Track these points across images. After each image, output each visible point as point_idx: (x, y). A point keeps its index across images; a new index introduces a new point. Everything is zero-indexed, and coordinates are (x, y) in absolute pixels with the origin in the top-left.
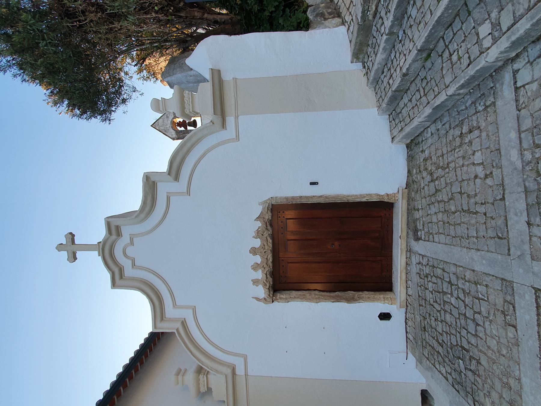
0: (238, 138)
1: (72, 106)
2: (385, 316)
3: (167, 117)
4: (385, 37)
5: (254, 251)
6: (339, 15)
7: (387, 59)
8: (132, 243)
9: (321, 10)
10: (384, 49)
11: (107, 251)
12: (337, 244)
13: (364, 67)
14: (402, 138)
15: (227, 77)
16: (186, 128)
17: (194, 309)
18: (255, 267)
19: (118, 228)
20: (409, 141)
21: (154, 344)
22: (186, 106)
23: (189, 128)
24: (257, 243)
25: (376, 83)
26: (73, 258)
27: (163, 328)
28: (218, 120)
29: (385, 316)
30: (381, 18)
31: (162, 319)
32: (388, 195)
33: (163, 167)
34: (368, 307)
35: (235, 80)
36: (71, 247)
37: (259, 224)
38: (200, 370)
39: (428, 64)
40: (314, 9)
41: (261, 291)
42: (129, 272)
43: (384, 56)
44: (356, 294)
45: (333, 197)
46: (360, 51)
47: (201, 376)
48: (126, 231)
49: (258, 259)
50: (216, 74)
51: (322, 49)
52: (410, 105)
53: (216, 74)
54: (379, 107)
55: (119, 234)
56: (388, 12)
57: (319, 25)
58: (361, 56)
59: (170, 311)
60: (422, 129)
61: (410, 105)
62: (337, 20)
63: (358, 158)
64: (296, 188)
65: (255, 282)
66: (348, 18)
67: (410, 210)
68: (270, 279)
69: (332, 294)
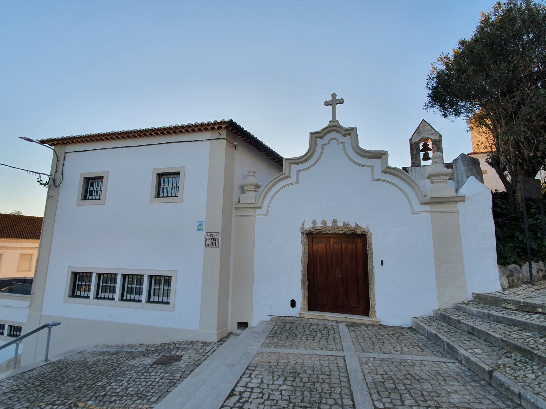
0: (414, 212)
1: (439, 76)
2: (293, 304)
3: (433, 134)
4: (486, 312)
5: (335, 221)
6: (510, 287)
7: (473, 314)
8: (339, 143)
9: (516, 274)
10: (479, 312)
11: (334, 127)
12: (340, 276)
13: (469, 302)
14: (416, 322)
15: (460, 206)
16: (422, 151)
17: (296, 183)
18: (324, 222)
19: (350, 134)
20: (414, 327)
21: (274, 160)
22: (437, 178)
23: (422, 154)
24: (340, 224)
25: (458, 308)
26: (327, 104)
27: (286, 165)
28: (426, 200)
29: (293, 304)
30: (502, 311)
31: (290, 163)
32: (375, 312)
33: (391, 164)
34: (299, 293)
35: (458, 212)
36: (334, 102)
37: (353, 225)
38: (257, 186)
39: (465, 333)
40: (517, 270)
41: (308, 226)
42: (320, 142)
43: (474, 312)
44: (307, 287)
45: (372, 275)
46: (480, 299)
47: (253, 187)
48: (347, 139)
49: (330, 224)
50: (463, 199)
51: (484, 274)
52: (439, 326)
53: (463, 199)
54: (439, 310)
55: (345, 135)
56: (503, 314)
57: (502, 273)
58: (477, 300)
59: (295, 168)
60: (422, 333)
61: (439, 326)
62: (506, 285)
63: (401, 293)
64: (378, 250)
65: (314, 222)
66: (507, 292)
67: (367, 325)
68: (316, 232)
69: (306, 271)
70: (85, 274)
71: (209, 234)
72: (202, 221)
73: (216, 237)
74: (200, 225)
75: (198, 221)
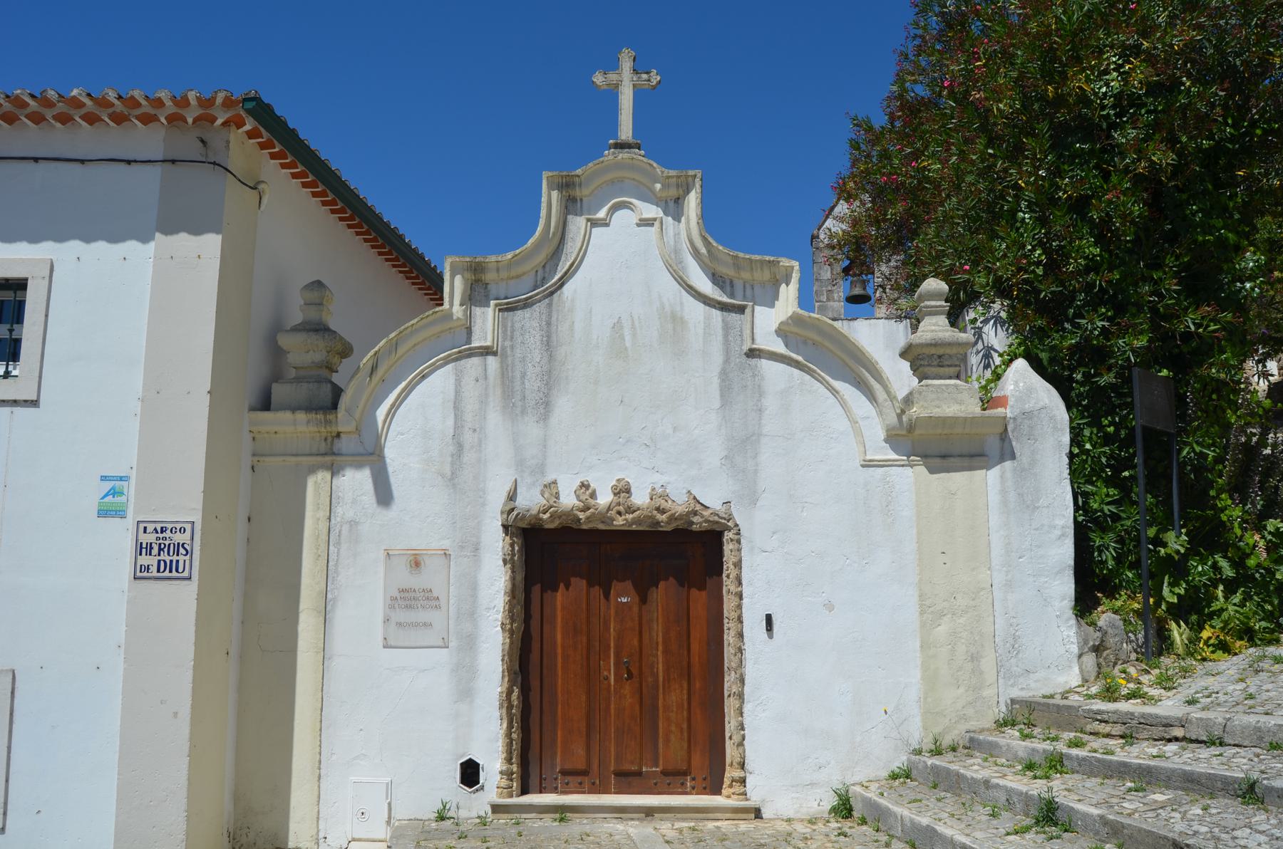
2: (470, 774)
5: (623, 490)
29: (470, 774)
41: (531, 501)
46: (1024, 715)
49: (604, 498)
51: (1050, 647)
70: (801, 828)
71: (150, 528)
72: (121, 479)
73: (179, 538)
74: (114, 492)
75: (104, 478)
